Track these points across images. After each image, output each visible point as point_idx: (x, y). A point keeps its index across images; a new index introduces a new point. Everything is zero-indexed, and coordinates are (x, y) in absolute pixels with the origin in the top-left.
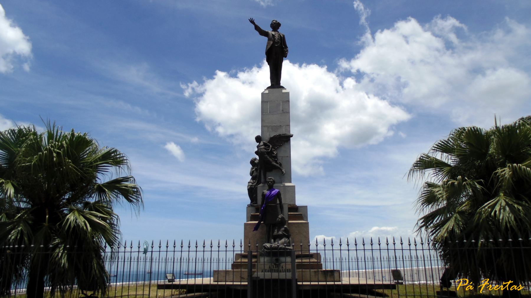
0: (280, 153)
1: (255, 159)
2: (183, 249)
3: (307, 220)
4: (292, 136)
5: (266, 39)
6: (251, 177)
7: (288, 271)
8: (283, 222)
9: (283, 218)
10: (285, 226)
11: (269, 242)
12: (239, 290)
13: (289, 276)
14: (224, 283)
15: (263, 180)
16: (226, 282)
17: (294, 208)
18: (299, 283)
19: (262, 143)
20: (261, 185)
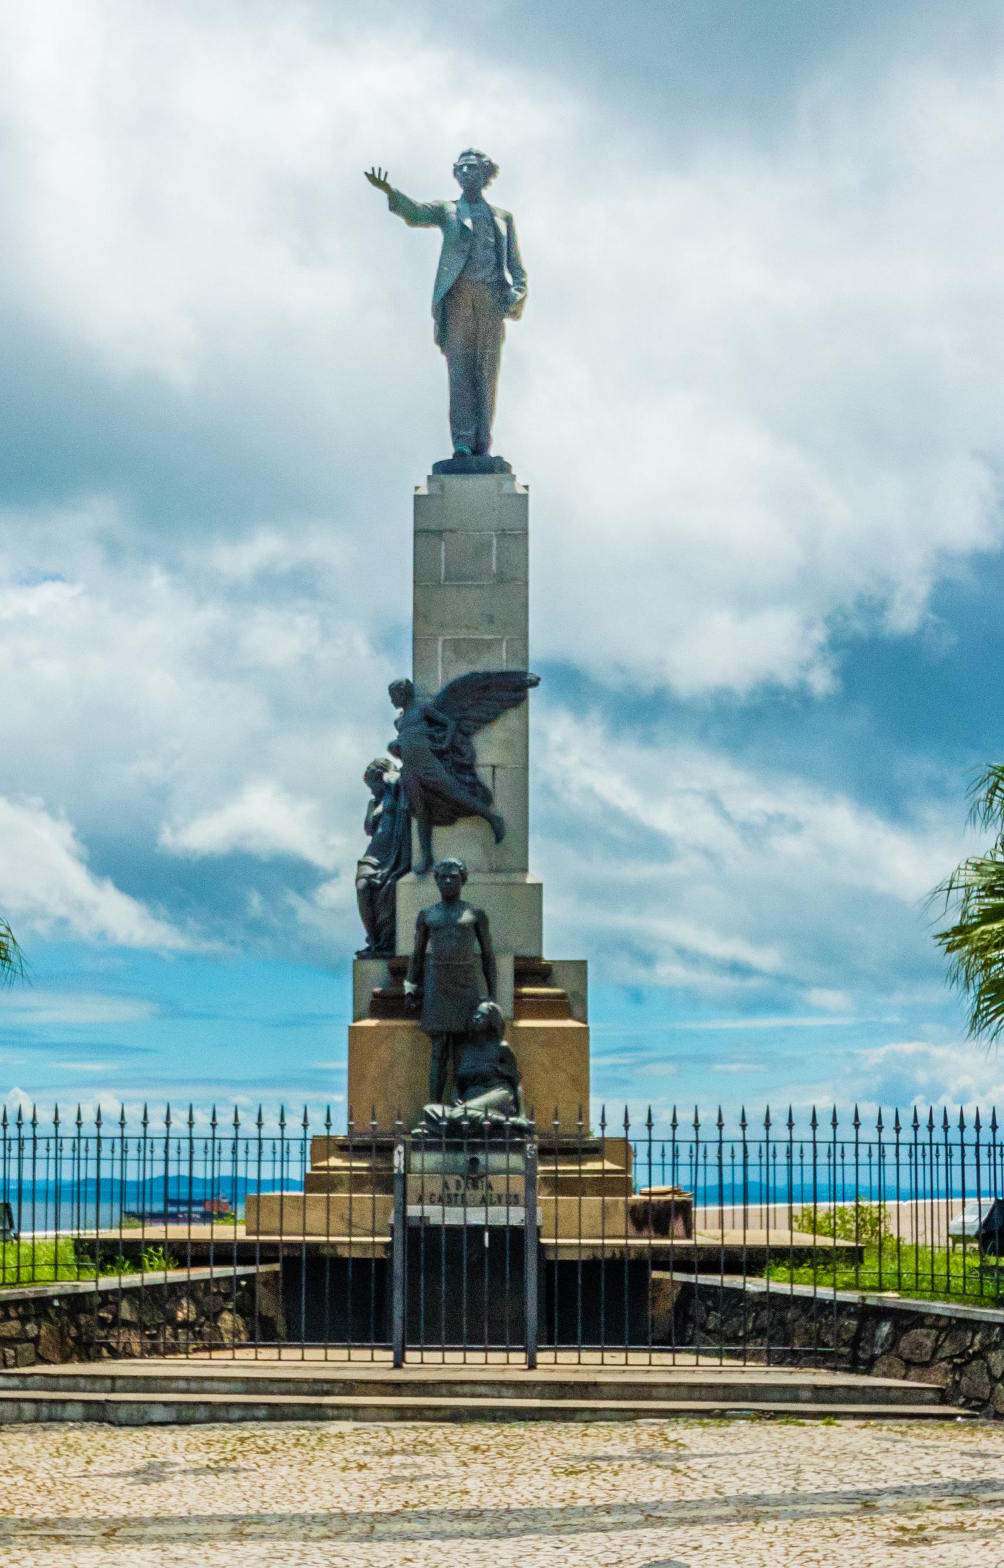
0: (488, 748)
1: (385, 767)
2: (250, 1157)
3: (583, 1019)
4: (535, 683)
5: (435, 235)
6: (369, 839)
7: (511, 1200)
8: (493, 1028)
9: (493, 1012)
10: (504, 1043)
11: (438, 1099)
12: (345, 1260)
13: (517, 1216)
14: (278, 1238)
15: (417, 857)
16: (328, 1235)
17: (532, 970)
18: (543, 1241)
19: (415, 713)
20: (410, 877)
